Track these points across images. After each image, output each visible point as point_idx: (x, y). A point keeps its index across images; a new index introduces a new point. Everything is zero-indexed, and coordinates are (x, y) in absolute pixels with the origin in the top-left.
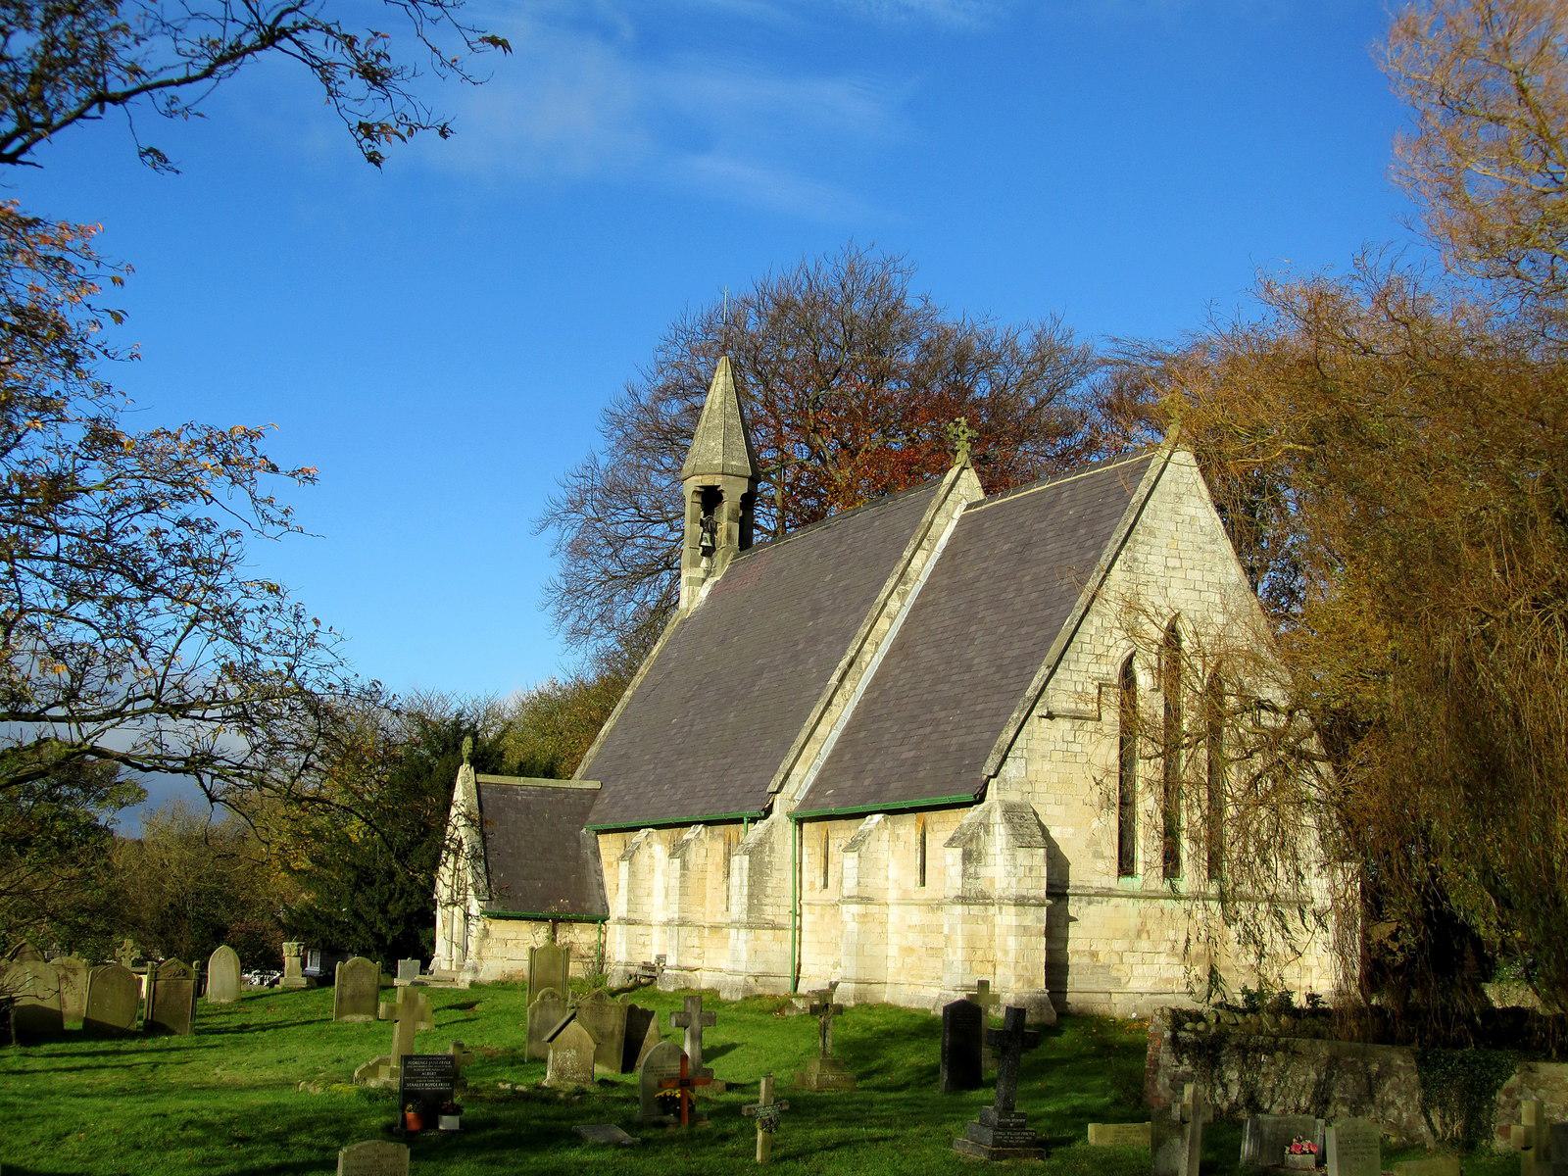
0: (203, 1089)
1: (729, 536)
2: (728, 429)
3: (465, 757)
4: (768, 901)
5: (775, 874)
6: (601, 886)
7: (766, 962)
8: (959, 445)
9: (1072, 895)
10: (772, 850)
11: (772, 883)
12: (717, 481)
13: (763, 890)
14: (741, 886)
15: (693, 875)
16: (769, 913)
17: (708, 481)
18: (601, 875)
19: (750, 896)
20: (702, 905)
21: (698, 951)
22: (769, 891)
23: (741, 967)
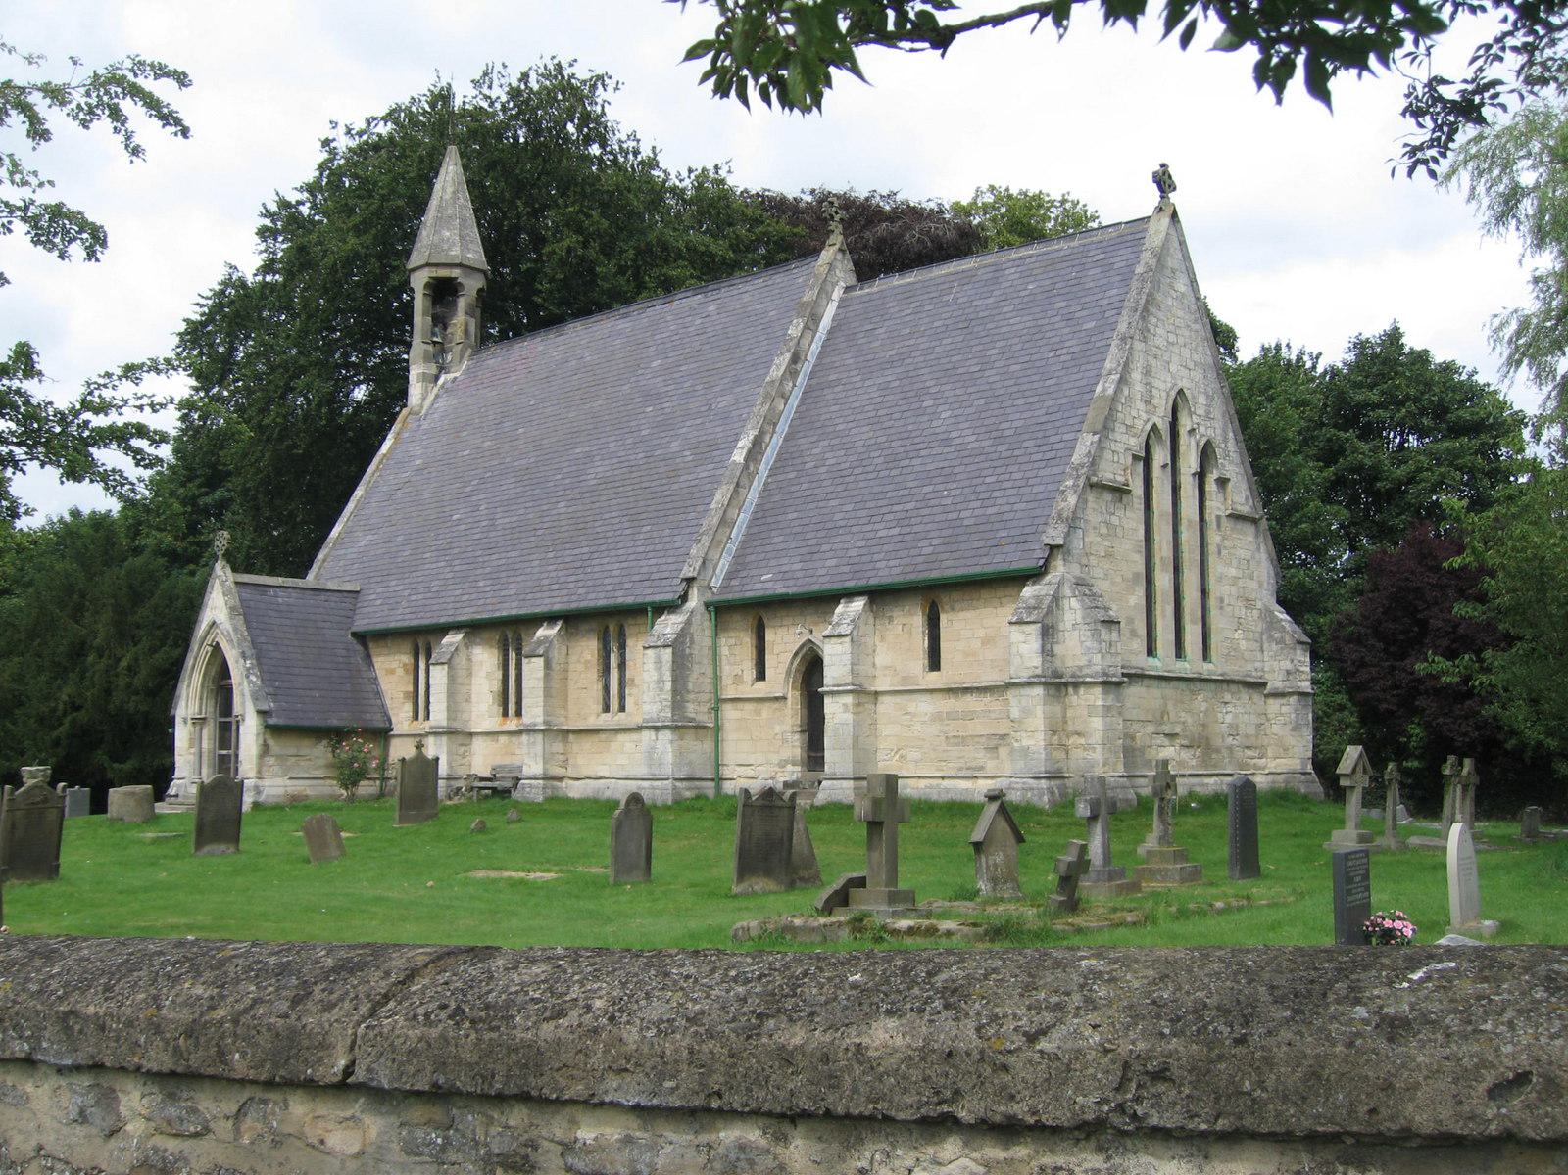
0: (440, 958)
1: (466, 332)
2: (463, 220)
3: (220, 554)
4: (692, 696)
5: (696, 667)
6: (379, 694)
7: (690, 763)
8: (833, 225)
9: (832, 693)
10: (692, 642)
11: (693, 676)
12: (455, 273)
13: (686, 682)
14: (660, 681)
15: (556, 675)
16: (691, 709)
17: (443, 273)
18: (378, 685)
19: (675, 692)
20: (565, 707)
21: (562, 757)
22: (690, 686)
23: (668, 770)
